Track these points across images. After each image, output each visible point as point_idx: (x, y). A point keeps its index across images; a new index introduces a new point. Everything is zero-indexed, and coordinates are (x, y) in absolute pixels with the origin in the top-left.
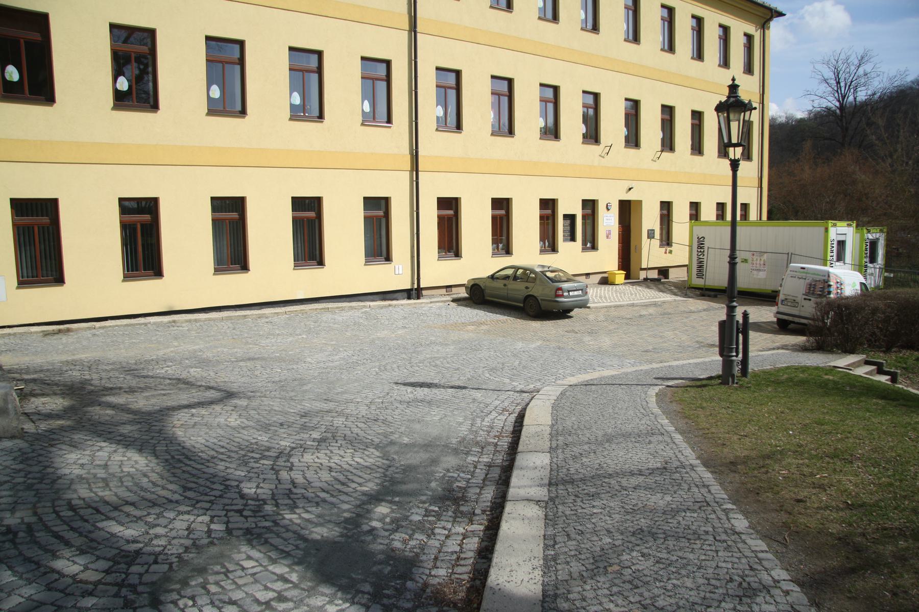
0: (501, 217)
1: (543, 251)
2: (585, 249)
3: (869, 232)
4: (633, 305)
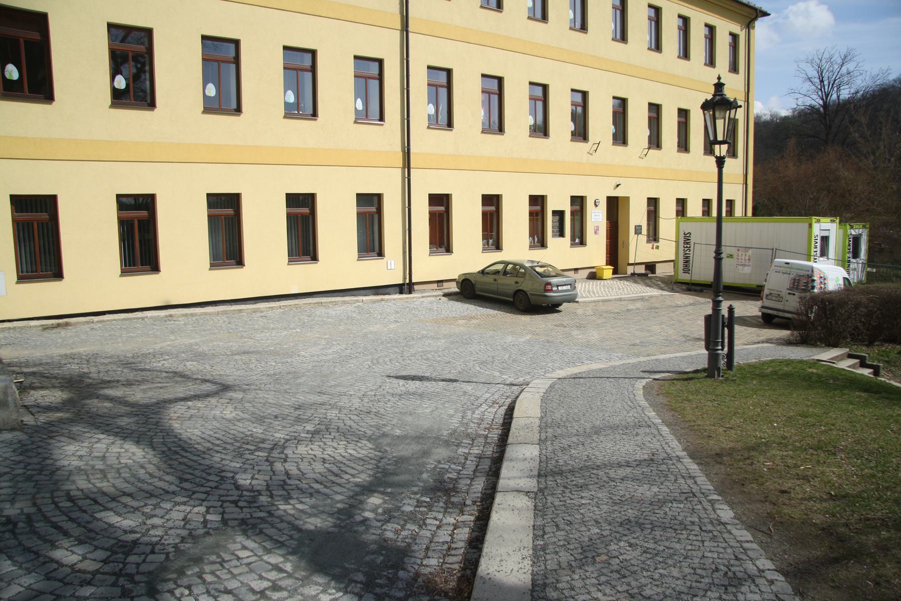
0: (491, 214)
1: (532, 247)
2: (573, 244)
3: (852, 227)
4: (620, 300)
